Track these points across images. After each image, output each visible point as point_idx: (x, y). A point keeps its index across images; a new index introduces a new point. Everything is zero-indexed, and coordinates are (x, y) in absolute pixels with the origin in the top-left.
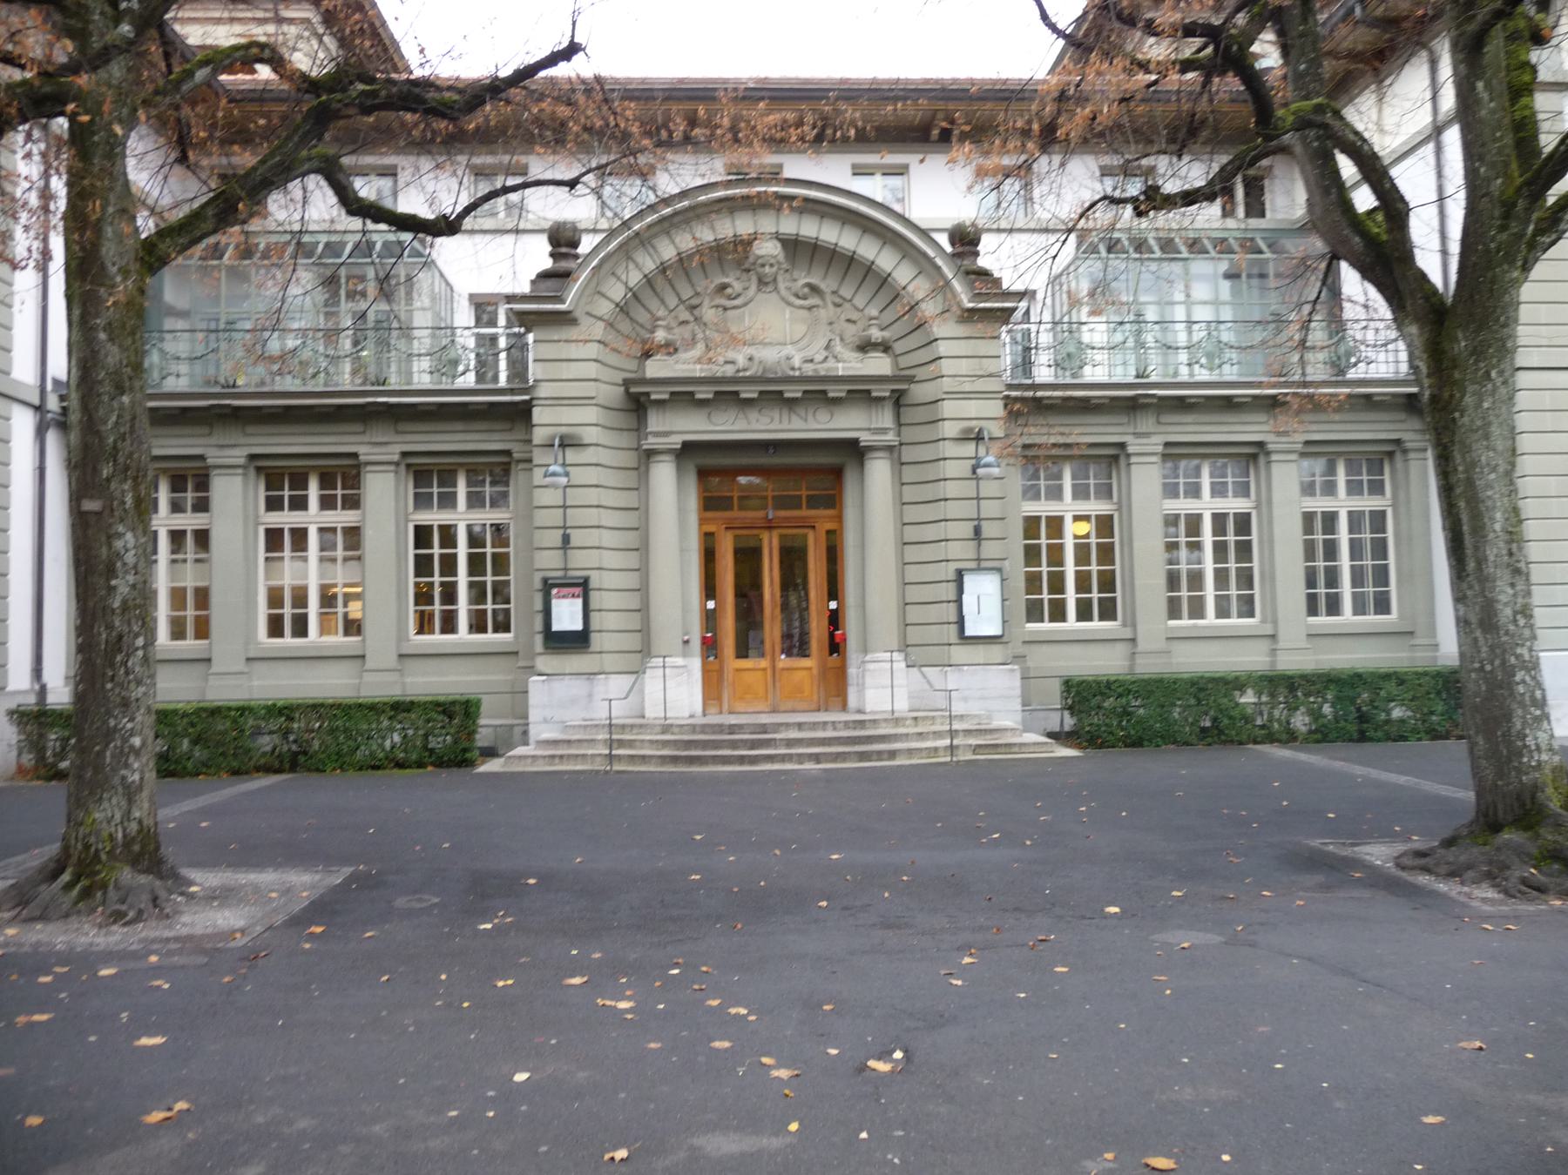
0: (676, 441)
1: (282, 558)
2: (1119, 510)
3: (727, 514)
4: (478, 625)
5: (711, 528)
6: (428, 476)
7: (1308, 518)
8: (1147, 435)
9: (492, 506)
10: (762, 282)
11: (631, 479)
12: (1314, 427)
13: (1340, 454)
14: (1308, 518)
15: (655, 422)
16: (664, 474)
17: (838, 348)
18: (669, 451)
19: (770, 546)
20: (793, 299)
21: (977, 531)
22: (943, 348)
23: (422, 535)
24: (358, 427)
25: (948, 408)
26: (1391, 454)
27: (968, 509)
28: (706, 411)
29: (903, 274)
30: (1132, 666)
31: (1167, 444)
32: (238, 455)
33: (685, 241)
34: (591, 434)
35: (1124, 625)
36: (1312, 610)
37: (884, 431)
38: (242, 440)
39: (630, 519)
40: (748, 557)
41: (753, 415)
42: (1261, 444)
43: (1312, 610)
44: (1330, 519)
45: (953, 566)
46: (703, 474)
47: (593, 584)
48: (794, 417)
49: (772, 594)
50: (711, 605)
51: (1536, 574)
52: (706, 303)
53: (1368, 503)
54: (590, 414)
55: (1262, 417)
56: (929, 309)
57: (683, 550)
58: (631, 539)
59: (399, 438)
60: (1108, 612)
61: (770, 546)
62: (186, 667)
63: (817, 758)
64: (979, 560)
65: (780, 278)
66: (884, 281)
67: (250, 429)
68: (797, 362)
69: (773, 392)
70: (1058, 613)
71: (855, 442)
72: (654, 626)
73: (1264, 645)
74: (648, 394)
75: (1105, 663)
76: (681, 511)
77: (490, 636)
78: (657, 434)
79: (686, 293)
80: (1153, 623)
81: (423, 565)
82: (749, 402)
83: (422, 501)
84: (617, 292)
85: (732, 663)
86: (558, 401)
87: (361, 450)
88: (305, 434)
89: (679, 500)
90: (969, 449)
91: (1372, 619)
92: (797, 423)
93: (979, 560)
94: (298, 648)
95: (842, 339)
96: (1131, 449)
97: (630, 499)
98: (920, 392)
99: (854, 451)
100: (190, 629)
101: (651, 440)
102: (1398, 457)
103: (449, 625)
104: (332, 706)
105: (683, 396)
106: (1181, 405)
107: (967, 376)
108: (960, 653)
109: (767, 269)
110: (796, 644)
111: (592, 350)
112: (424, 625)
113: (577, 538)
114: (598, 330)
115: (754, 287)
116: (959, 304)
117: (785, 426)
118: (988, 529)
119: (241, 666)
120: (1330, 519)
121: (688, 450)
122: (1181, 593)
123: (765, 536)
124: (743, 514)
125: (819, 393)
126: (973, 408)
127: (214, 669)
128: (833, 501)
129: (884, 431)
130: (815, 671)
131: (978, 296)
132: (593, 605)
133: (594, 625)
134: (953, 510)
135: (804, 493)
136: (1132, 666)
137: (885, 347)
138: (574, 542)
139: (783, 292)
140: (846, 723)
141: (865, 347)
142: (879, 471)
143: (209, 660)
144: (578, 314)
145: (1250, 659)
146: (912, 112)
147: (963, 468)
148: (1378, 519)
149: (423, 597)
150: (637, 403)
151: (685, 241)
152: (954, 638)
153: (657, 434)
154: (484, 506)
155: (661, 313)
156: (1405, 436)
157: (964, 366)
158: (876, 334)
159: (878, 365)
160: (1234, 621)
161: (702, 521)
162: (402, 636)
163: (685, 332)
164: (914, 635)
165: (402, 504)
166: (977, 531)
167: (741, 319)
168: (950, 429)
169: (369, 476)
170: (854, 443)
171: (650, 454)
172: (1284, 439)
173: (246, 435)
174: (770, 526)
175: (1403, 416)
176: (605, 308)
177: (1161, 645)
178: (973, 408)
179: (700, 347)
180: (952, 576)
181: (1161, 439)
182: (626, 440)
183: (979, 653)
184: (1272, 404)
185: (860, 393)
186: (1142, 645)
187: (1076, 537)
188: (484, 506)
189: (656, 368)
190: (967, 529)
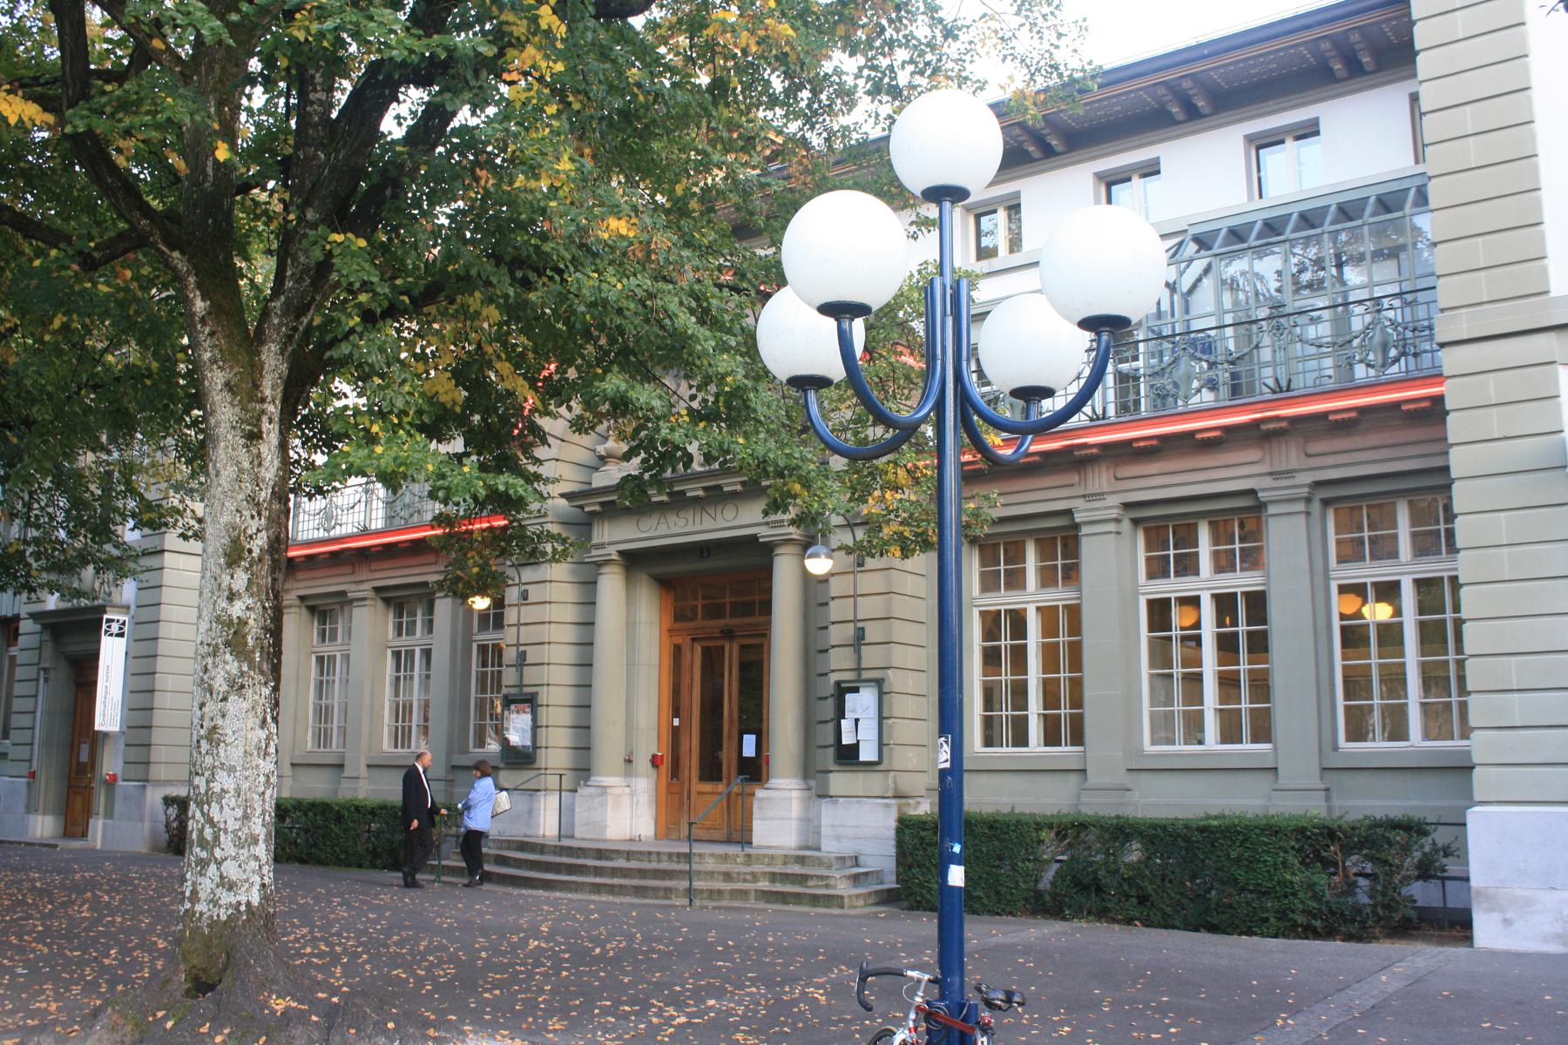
3: (692, 624)
5: (678, 640)
6: (1166, 532)
8: (1100, 496)
9: (1177, 574)
13: (1029, 533)
16: (611, 585)
21: (860, 635)
23: (1159, 611)
30: (1330, 809)
41: (672, 518)
47: (543, 699)
48: (705, 516)
49: (730, 709)
50: (676, 722)
51: (1475, 674)
55: (1253, 454)
60: (1262, 731)
67: (374, 566)
71: (754, 538)
82: (734, 495)
85: (699, 787)
92: (708, 523)
93: (859, 669)
94: (403, 757)
96: (1078, 518)
100: (1007, 732)
101: (594, 552)
103: (1021, 739)
104: (373, 812)
112: (1357, 731)
117: (698, 527)
121: (633, 561)
127: (346, 774)
132: (543, 721)
133: (542, 742)
136: (336, 791)
140: (670, 855)
143: (341, 766)
146: (1214, 48)
154: (1363, 559)
165: (1318, 552)
169: (1270, 520)
172: (1285, 483)
186: (1093, 778)
187: (1343, 617)
188: (1363, 559)
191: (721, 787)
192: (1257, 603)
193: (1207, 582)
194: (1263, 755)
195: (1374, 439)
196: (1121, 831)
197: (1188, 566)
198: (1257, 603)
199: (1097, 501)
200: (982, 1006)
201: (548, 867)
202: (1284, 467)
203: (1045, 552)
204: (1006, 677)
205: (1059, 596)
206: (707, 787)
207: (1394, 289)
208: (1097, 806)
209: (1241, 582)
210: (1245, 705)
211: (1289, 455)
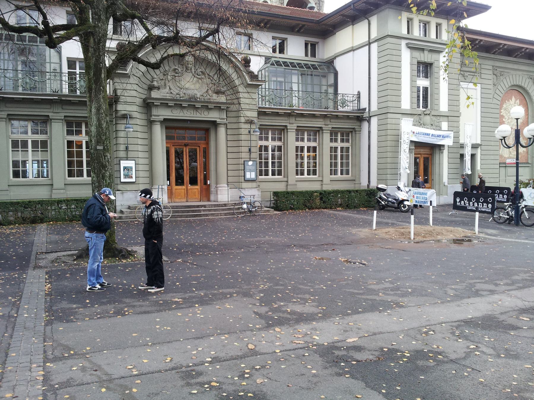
0: (161, 118)
1: (19, 151)
2: (284, 144)
3: (174, 141)
5: (169, 145)
7: (297, 147)
8: (293, 124)
10: (187, 69)
12: (334, 124)
13: (339, 131)
14: (297, 147)
15: (155, 111)
19: (186, 151)
21: (250, 150)
23: (70, 144)
24: (48, 106)
26: (351, 132)
28: (171, 109)
30: (322, 188)
31: (298, 126)
32: (62, 115)
34: (135, 115)
35: (284, 177)
36: (297, 174)
37: (223, 119)
38: (5, 109)
40: (179, 155)
41: (185, 111)
42: (321, 128)
43: (297, 174)
44: (336, 148)
45: (243, 160)
46: (167, 128)
49: (187, 166)
53: (345, 145)
54: (135, 108)
55: (321, 120)
56: (237, 82)
57: (163, 152)
59: (7, 109)
60: (280, 174)
61: (186, 151)
62: (84, 186)
63: (225, 214)
64: (127, 157)
67: (8, 105)
68: (198, 96)
69: (192, 103)
70: (267, 174)
73: (320, 183)
74: (153, 103)
75: (281, 187)
76: (162, 140)
77: (276, 177)
80: (293, 177)
81: (70, 154)
82: (211, 109)
83: (69, 133)
85: (175, 187)
86: (126, 103)
87: (50, 114)
88: (28, 108)
90: (247, 126)
91: (345, 176)
99: (215, 124)
100: (344, 172)
102: (354, 133)
103: (302, 174)
105: (164, 104)
106: (302, 115)
107: (250, 103)
108: (245, 185)
110: (193, 181)
113: (131, 148)
116: (246, 82)
117: (195, 115)
119: (7, 188)
120: (336, 148)
121: (165, 121)
124: (178, 141)
128: (207, 139)
129: (223, 119)
130: (199, 190)
131: (251, 81)
136: (322, 188)
141: (218, 92)
142: (222, 131)
145: (315, 187)
147: (247, 132)
148: (348, 148)
149: (70, 164)
150: (148, 105)
152: (243, 181)
155: (155, 76)
156: (356, 127)
159: (222, 99)
160: (311, 176)
162: (65, 179)
164: (230, 179)
166: (250, 150)
173: (6, 107)
174: (186, 145)
175: (356, 122)
177: (294, 182)
180: (243, 163)
181: (6, 113)
183: (250, 185)
184: (325, 117)
186: (289, 183)
189: (155, 94)
190: (247, 149)
191: (184, 187)
193: (270, 144)
194: (315, 178)
196: (68, 202)
199: (293, 125)
201: (183, 212)
202: (157, 114)
203: (342, 135)
204: (299, 161)
205: (278, 143)
207: (267, 87)
210: (21, 169)
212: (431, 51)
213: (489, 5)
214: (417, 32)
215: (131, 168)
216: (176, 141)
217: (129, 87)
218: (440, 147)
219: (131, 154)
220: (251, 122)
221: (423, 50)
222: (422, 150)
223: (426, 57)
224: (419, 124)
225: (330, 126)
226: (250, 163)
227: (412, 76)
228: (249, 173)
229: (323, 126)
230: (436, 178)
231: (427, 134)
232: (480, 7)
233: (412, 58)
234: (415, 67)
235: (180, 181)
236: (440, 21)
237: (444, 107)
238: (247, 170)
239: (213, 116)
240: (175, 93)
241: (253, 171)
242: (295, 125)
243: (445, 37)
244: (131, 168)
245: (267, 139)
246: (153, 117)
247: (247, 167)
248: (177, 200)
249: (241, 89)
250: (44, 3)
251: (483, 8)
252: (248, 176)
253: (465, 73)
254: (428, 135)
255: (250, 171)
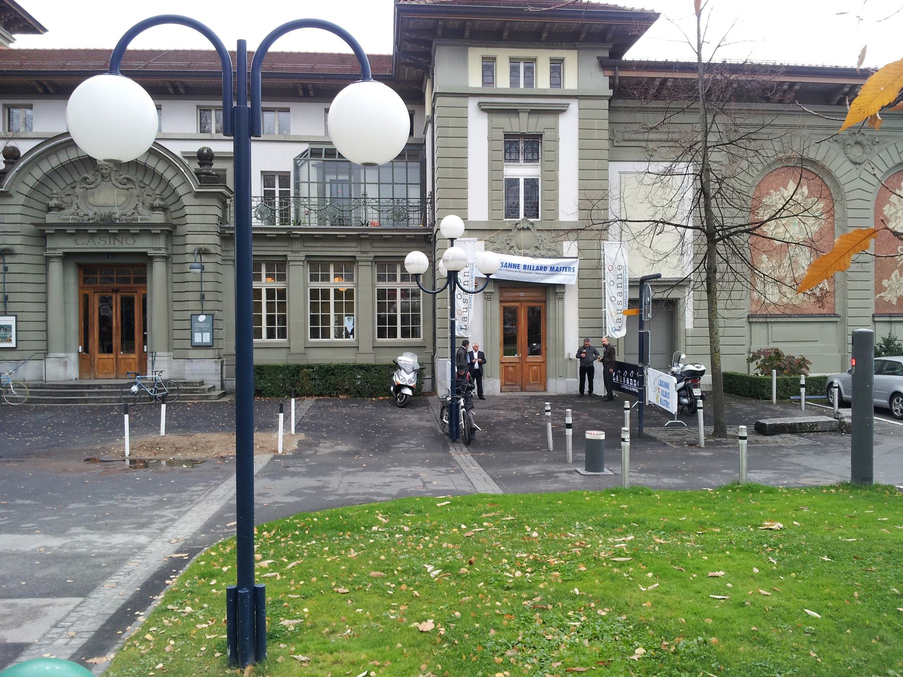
0: (60, 252)
4: (405, 334)
5: (87, 292)
11: (41, 269)
15: (50, 243)
16: (55, 268)
17: (140, 208)
18: (58, 257)
20: (119, 185)
21: (203, 297)
22: (187, 210)
25: (190, 239)
27: (196, 286)
29: (169, 175)
33: (55, 162)
34: (18, 249)
39: (41, 288)
41: (97, 240)
45: (190, 313)
48: (116, 242)
49: (117, 323)
52: (78, 186)
55: (354, 244)
56: (181, 191)
58: (41, 297)
60: (283, 334)
61: (116, 300)
64: (6, 312)
65: (112, 175)
66: (161, 178)
69: (105, 226)
71: (146, 253)
72: (50, 339)
78: (50, 249)
79: (69, 181)
84: (31, 181)
85: (98, 356)
89: (64, 281)
91: (411, 340)
92: (118, 244)
93: (202, 310)
95: (143, 204)
97: (42, 279)
98: (180, 230)
101: (48, 251)
103: (326, 334)
105: (61, 231)
108: (193, 353)
109: (104, 171)
111: (19, 209)
113: (11, 297)
114: (21, 200)
115: (100, 179)
117: (112, 245)
118: (208, 296)
121: (67, 257)
122: (318, 327)
123: (114, 296)
125: (126, 230)
126: (201, 239)
129: (159, 249)
131: (200, 187)
134: (190, 287)
135: (132, 276)
137: (164, 209)
138: (10, 299)
139: (114, 182)
141: (153, 208)
142: (158, 270)
144: (11, 192)
151: (55, 162)
152: (190, 347)
153: (50, 249)
157: (198, 219)
158: (157, 202)
159: (158, 218)
160: (277, 340)
161: (81, 288)
162: (374, 340)
163: (67, 199)
166: (203, 297)
167: (93, 194)
168: (190, 249)
170: (145, 254)
171: (48, 259)
174: (116, 291)
176: (26, 190)
177: (302, 350)
178: (201, 239)
179: (75, 206)
182: (38, 251)
183: (202, 353)
184: (358, 239)
185: (146, 231)
189: (51, 218)
190: (197, 296)
191: (112, 356)
192: (282, 294)
195: (395, 245)
197: (326, 278)
198: (282, 294)
199: (296, 255)
200: (762, 506)
206: (105, 356)
208: (293, 361)
209: (277, 285)
211: (367, 247)
212: (533, 112)
213: (657, 11)
214: (503, 81)
215: (10, 327)
216: (99, 285)
217: (11, 209)
218: (557, 290)
219: (11, 307)
220: (203, 252)
221: (516, 112)
222: (522, 294)
223: (524, 124)
224: (508, 247)
225: (373, 254)
226: (202, 318)
227: (492, 161)
228: (200, 334)
229: (358, 254)
230: (550, 344)
231: (521, 265)
232: (645, 19)
233: (491, 128)
234: (501, 145)
235: (106, 347)
236: (558, 54)
237: (568, 209)
238: (196, 330)
239: (142, 245)
240: (82, 214)
241: (207, 332)
242: (303, 254)
243: (571, 82)
244: (10, 327)
245: (326, 278)
246: (48, 251)
247: (196, 325)
248: (101, 376)
249: (187, 200)
250: (208, 52)
251: (645, 19)
252: (198, 338)
253: (619, 144)
254: (516, 266)
255: (202, 331)
